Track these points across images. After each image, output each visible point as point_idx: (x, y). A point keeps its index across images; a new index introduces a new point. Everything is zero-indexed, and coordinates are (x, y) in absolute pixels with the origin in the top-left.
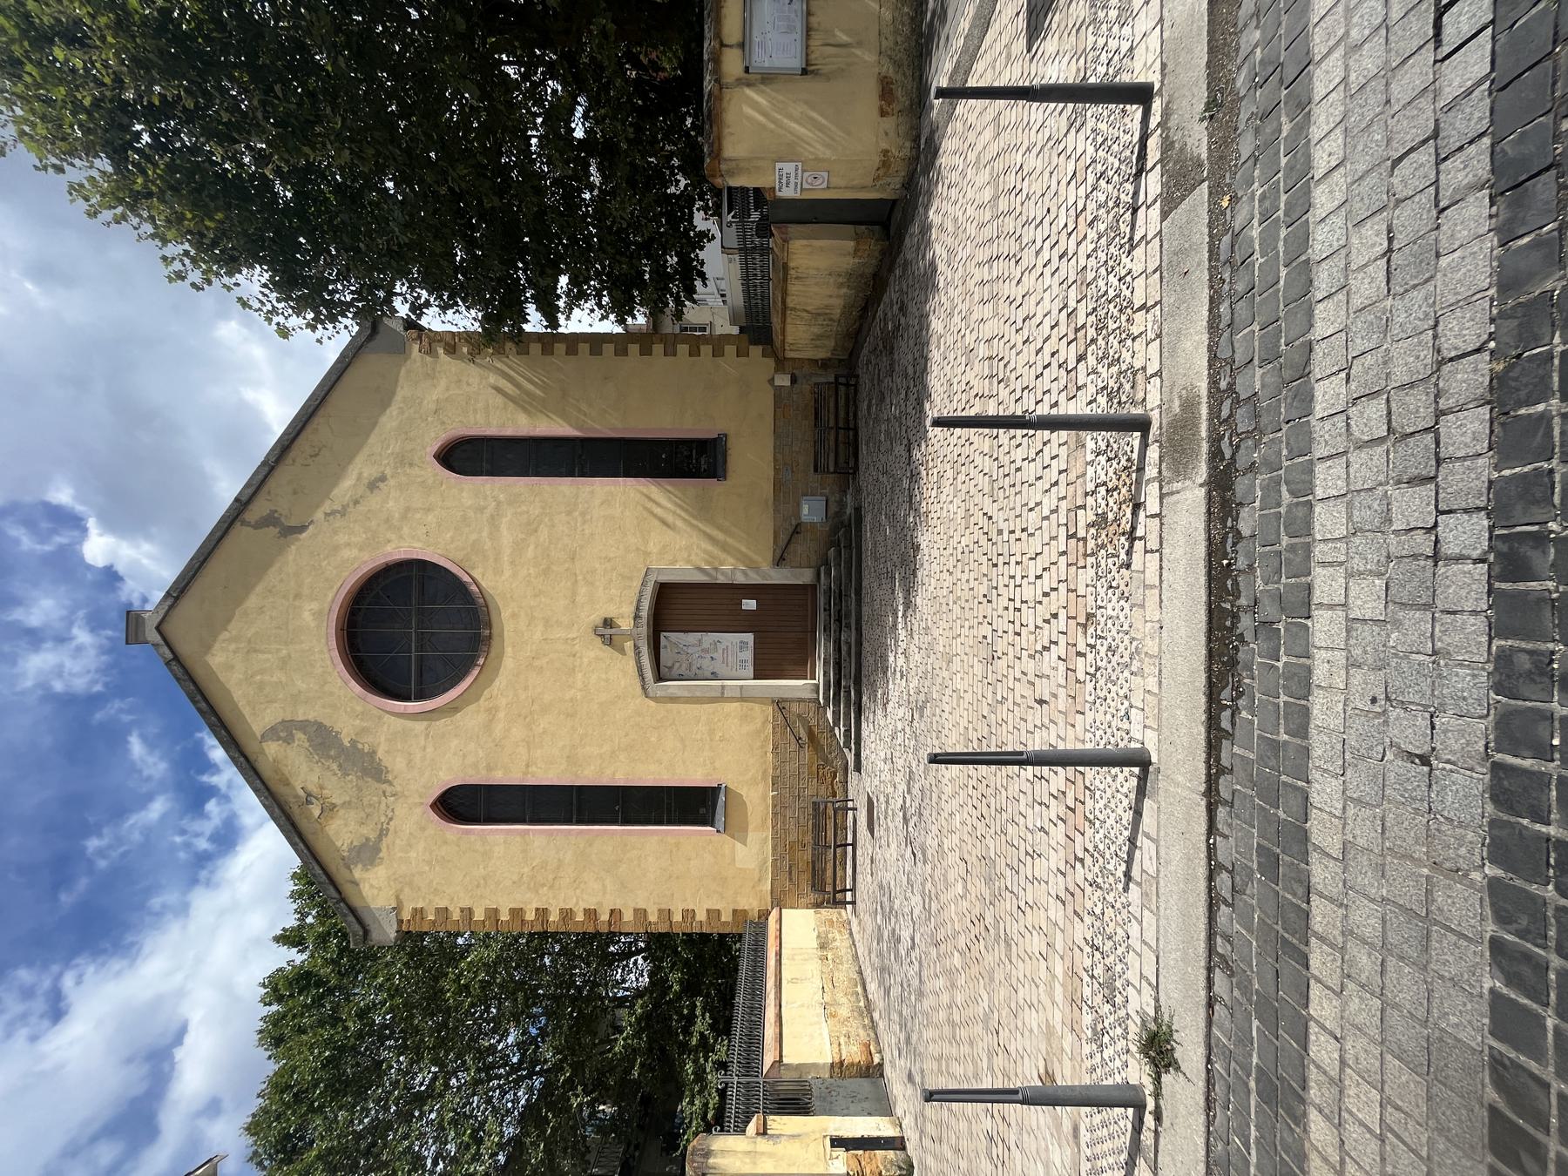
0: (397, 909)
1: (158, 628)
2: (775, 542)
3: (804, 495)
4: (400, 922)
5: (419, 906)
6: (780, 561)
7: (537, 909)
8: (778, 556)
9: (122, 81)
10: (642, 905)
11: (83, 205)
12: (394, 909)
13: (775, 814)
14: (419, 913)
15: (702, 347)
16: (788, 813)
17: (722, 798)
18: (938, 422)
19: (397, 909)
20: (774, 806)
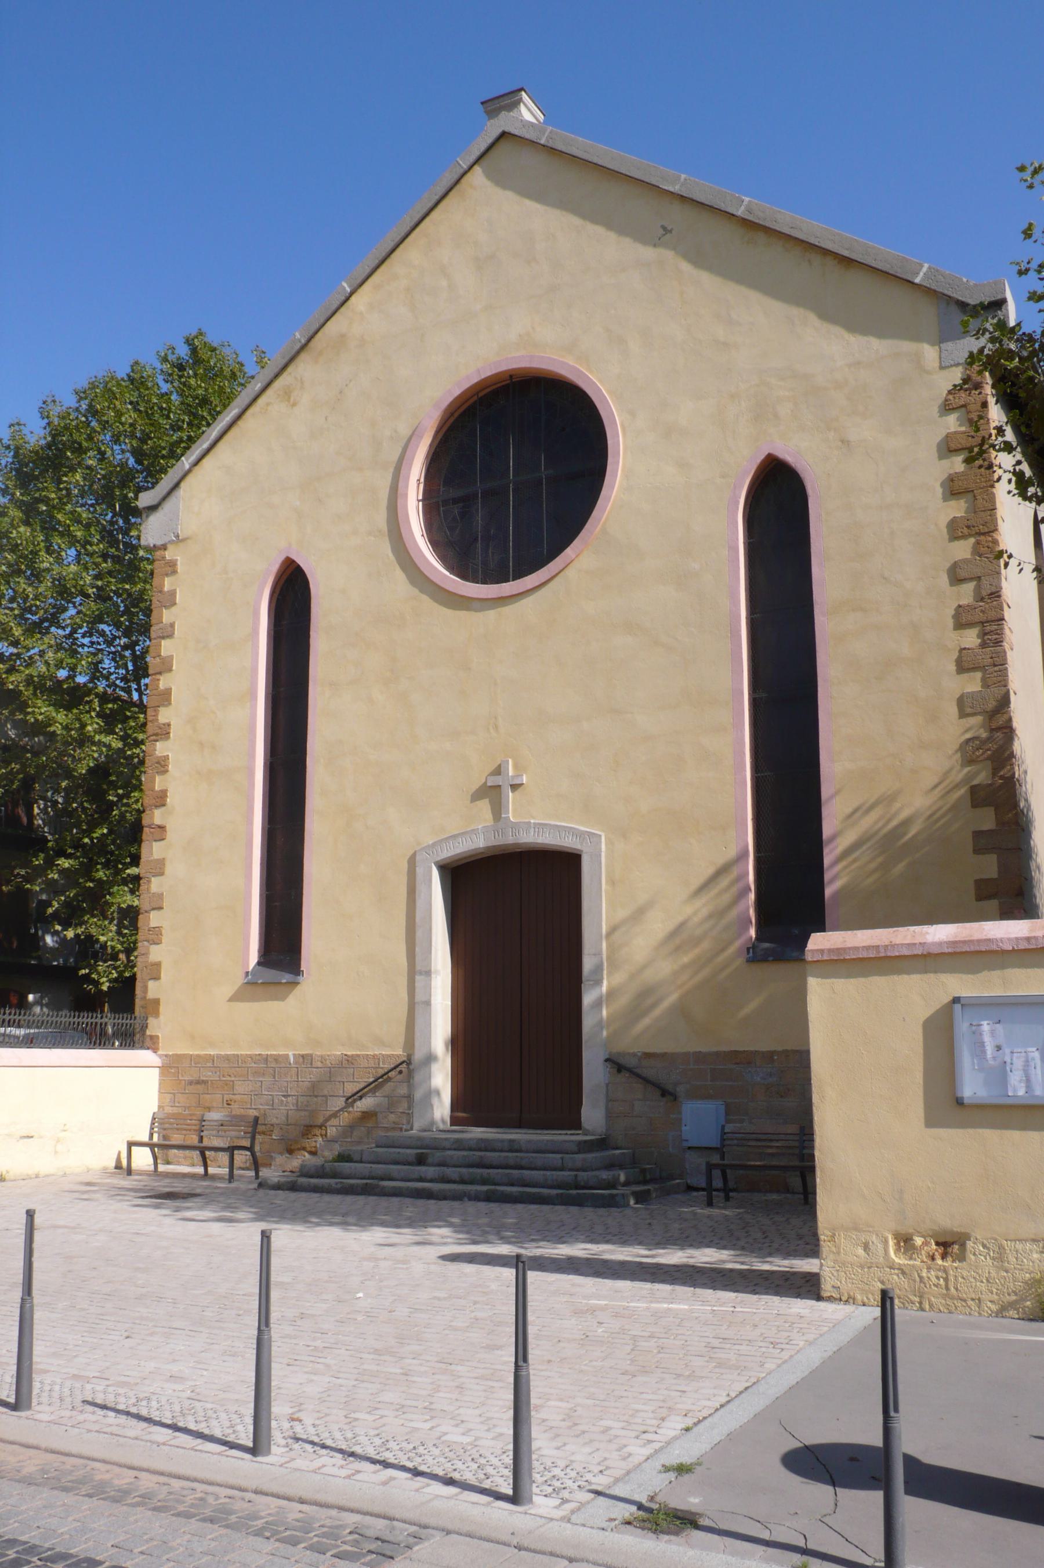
0: (178, 540)
1: (504, 135)
2: (648, 1056)
3: (728, 1106)
4: (164, 547)
5: (180, 568)
6: (616, 1064)
7: (169, 725)
8: (621, 1061)
9: (235, 375)
10: (168, 869)
11: (208, 339)
12: (177, 536)
13: (266, 1059)
14: (172, 568)
15: (152, 925)
16: (267, 1079)
17: (286, 977)
18: (266, 1236)
19: (178, 540)
20: (276, 1059)
